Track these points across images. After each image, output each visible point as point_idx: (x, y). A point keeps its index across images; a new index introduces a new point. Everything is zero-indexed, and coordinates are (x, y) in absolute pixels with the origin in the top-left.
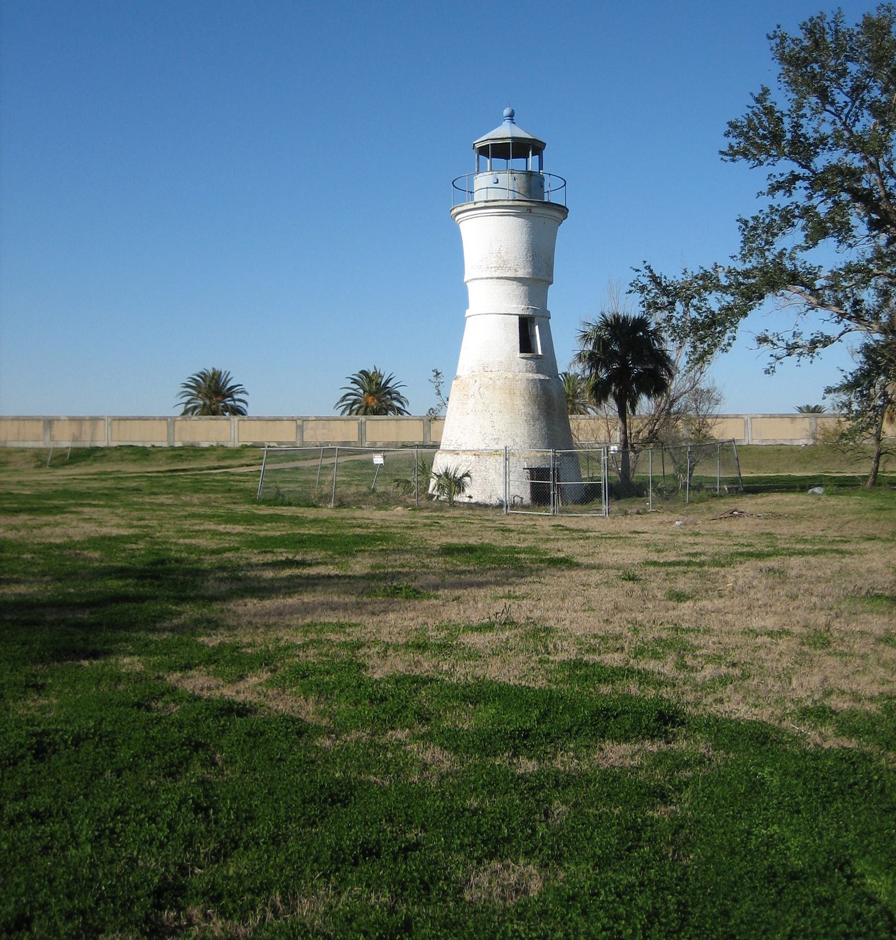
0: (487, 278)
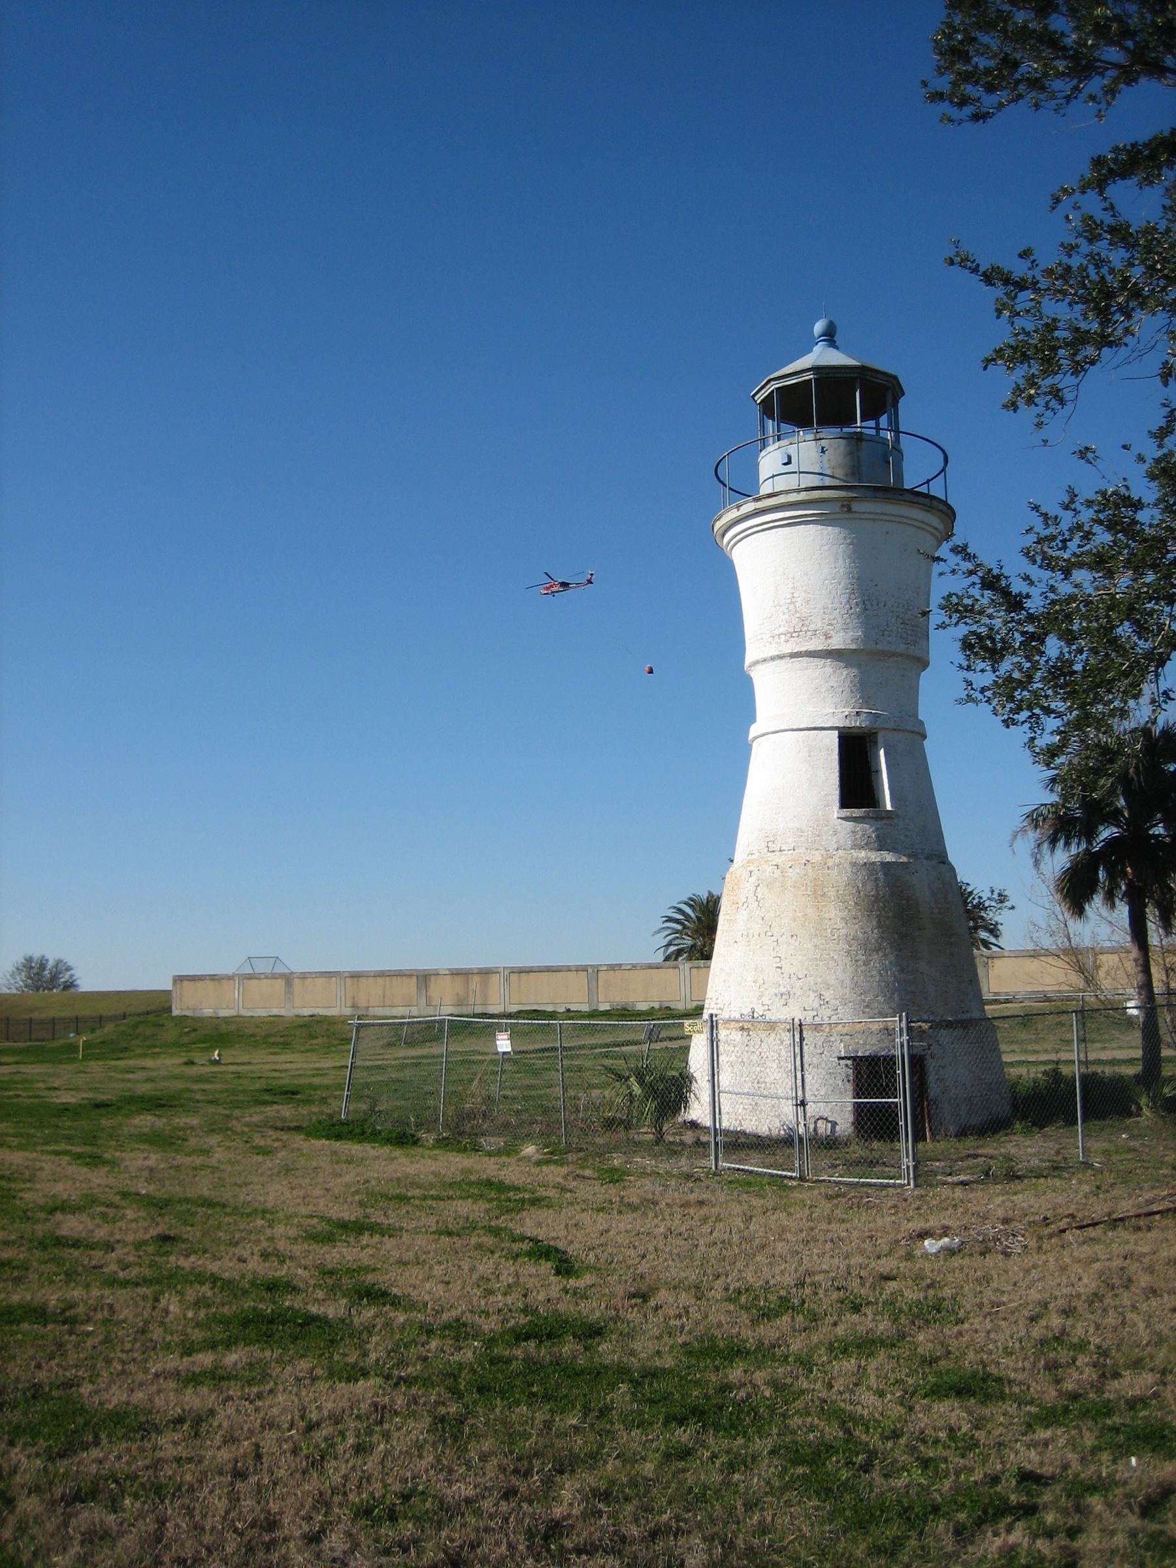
0: (773, 659)
